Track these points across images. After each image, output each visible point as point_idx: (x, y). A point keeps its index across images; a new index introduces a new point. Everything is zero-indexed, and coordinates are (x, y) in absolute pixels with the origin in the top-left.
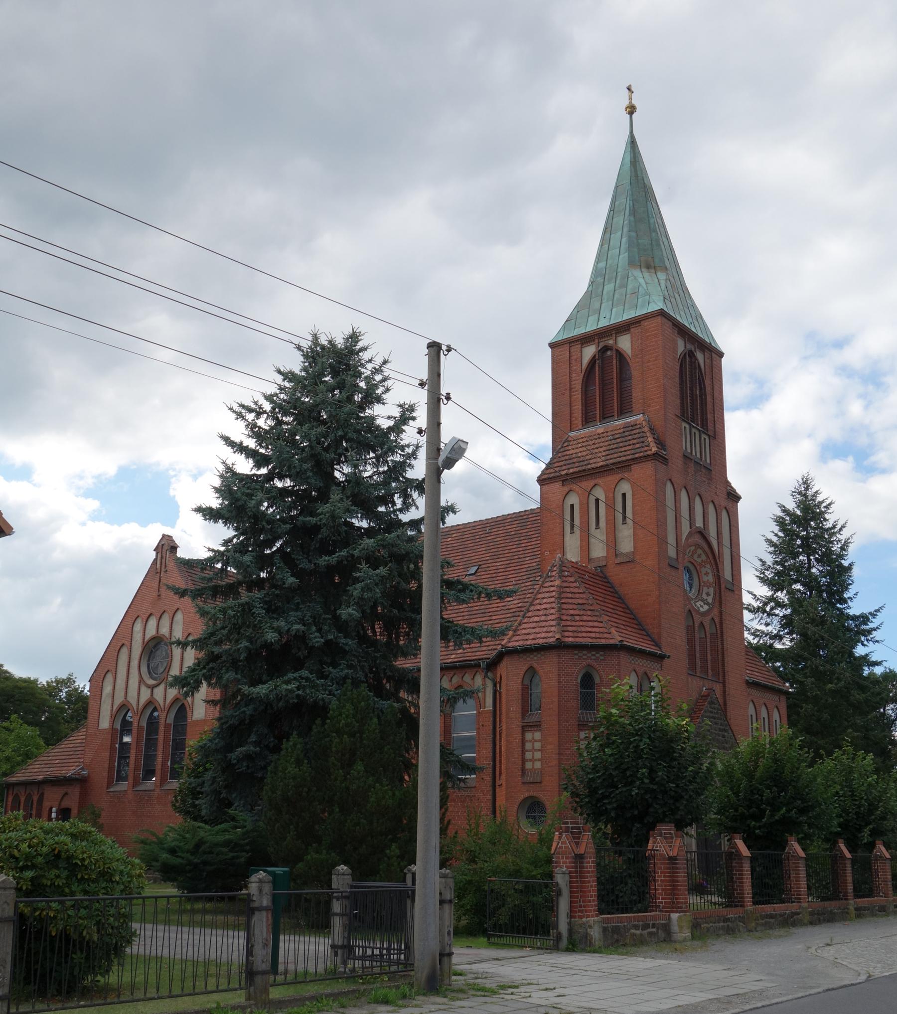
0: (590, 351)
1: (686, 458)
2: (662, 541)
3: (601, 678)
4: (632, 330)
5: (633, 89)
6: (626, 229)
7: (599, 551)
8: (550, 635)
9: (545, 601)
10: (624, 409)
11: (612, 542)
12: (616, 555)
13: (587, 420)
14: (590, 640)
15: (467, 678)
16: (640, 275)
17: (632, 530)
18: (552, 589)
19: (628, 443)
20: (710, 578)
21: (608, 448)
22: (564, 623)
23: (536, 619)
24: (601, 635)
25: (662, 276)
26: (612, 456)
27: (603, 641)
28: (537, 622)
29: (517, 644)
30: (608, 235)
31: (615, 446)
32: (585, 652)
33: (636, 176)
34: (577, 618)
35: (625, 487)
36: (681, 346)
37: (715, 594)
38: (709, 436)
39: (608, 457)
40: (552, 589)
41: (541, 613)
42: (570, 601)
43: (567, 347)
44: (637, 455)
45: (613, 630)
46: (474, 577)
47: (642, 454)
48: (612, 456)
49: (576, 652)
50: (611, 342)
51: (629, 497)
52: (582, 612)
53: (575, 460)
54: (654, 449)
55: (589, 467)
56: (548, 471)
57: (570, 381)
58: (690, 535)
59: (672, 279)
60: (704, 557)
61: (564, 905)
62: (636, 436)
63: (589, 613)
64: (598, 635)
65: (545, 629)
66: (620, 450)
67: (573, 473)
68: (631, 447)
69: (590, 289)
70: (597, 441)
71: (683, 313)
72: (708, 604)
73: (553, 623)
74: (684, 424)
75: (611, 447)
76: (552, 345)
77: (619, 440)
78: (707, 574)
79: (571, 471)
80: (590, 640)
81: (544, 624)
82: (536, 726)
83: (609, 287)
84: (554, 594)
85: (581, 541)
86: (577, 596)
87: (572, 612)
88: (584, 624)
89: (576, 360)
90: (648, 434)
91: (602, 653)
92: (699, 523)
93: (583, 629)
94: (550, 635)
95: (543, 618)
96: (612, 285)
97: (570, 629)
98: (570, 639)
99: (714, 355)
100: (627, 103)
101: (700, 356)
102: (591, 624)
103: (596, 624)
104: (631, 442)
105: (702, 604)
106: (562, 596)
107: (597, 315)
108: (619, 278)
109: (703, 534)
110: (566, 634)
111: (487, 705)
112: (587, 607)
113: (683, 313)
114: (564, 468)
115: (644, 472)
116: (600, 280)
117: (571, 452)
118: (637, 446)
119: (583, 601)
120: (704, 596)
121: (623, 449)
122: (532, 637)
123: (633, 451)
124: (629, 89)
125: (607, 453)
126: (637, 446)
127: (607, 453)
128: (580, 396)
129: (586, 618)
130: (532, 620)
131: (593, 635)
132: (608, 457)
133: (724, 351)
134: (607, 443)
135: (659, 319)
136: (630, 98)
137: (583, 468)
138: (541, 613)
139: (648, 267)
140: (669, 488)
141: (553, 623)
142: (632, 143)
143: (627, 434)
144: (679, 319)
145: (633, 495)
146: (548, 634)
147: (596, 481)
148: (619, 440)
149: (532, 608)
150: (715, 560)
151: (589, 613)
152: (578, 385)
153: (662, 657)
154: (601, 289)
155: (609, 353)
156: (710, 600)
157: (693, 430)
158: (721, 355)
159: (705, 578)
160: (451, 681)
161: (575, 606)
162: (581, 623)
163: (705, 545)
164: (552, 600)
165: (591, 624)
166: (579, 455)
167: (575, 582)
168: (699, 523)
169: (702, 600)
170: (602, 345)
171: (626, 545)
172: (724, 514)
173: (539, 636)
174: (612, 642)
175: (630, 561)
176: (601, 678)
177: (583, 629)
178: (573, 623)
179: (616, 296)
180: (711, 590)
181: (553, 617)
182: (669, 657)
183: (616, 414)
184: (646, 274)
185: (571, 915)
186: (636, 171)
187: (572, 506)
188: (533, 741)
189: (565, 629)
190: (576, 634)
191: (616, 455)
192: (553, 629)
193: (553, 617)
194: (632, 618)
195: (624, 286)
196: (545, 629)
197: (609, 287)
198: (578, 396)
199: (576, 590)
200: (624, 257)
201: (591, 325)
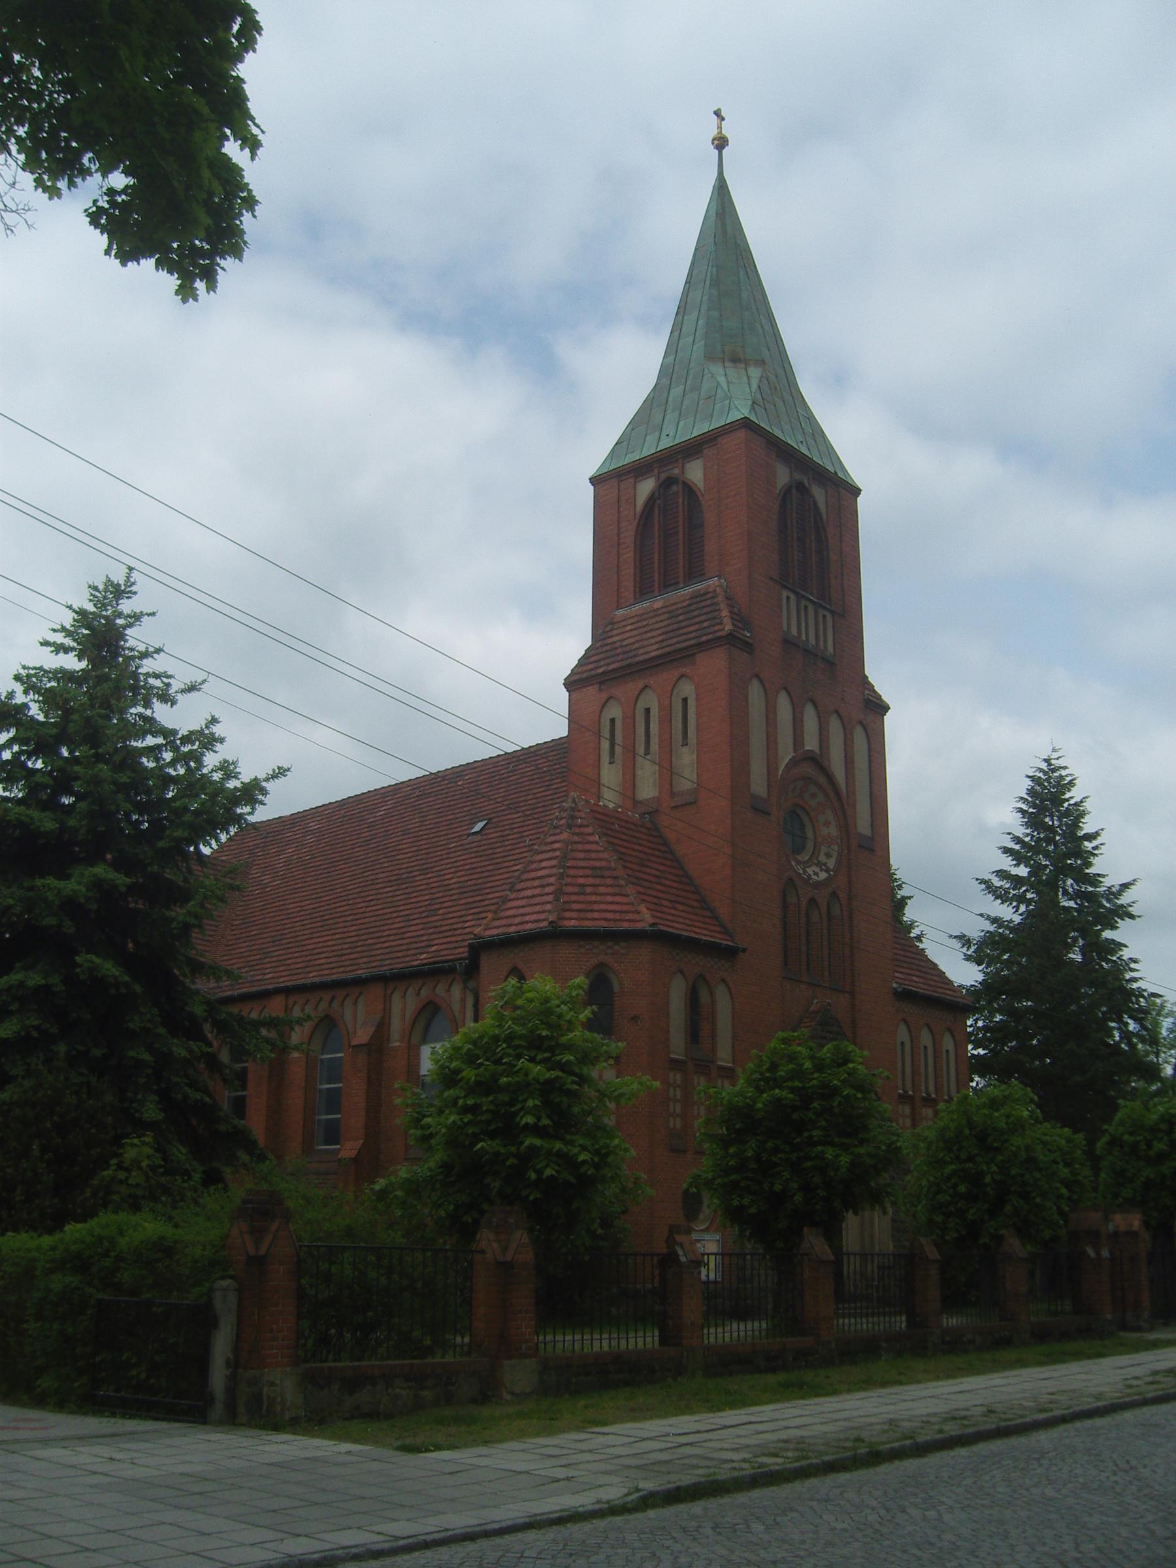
0: (646, 487)
1: (788, 643)
2: (740, 770)
4: (705, 451)
5: (723, 114)
7: (647, 790)
8: (543, 916)
9: (544, 864)
10: (694, 572)
11: (668, 771)
13: (643, 590)
14: (605, 924)
16: (721, 371)
18: (556, 846)
19: (692, 621)
20: (833, 830)
22: (566, 898)
23: (529, 893)
25: (755, 373)
26: (670, 642)
27: (625, 926)
29: (495, 932)
31: (676, 626)
32: (610, 944)
33: (725, 233)
35: (687, 689)
36: (783, 476)
38: (832, 612)
39: (664, 644)
40: (556, 846)
41: (536, 883)
42: (582, 864)
45: (643, 908)
46: (479, 837)
47: (710, 637)
48: (670, 642)
49: (582, 943)
50: (676, 471)
51: (692, 703)
52: (598, 881)
53: (618, 651)
54: (728, 627)
55: (636, 659)
58: (794, 763)
59: (772, 378)
61: (221, 1345)
64: (618, 916)
65: (537, 908)
66: (682, 631)
67: (613, 670)
68: (697, 627)
70: (651, 621)
71: (787, 427)
73: (550, 898)
74: (785, 593)
75: (671, 628)
76: (593, 480)
77: (681, 618)
79: (611, 667)
80: (605, 924)
81: (537, 900)
83: (676, 391)
84: (558, 853)
87: (581, 881)
90: (722, 606)
91: (623, 944)
93: (595, 907)
94: (543, 916)
97: (575, 906)
98: (573, 923)
99: (843, 491)
100: (715, 132)
101: (818, 494)
102: (610, 899)
104: (698, 620)
105: (817, 870)
107: (657, 433)
108: (690, 377)
109: (817, 761)
112: (607, 873)
113: (787, 427)
114: (602, 663)
118: (706, 624)
120: (822, 858)
121: (685, 631)
122: (517, 920)
124: (717, 113)
125: (664, 637)
126: (706, 624)
127: (664, 637)
128: (631, 554)
129: (602, 890)
130: (523, 894)
131: (608, 915)
132: (664, 644)
133: (859, 484)
134: (665, 623)
135: (741, 434)
136: (720, 128)
137: (629, 661)
138: (536, 883)
139: (735, 360)
140: (755, 691)
142: (721, 190)
143: (693, 607)
144: (778, 433)
145: (698, 699)
148: (681, 618)
149: (525, 877)
150: (842, 804)
153: (731, 953)
155: (674, 488)
156: (831, 863)
157: (803, 603)
158: (856, 491)
159: (824, 831)
160: (418, 994)
161: (587, 872)
162: (594, 898)
163: (822, 780)
164: (554, 862)
165: (610, 899)
166: (625, 643)
167: (592, 834)
169: (819, 864)
170: (663, 476)
172: (859, 733)
173: (527, 918)
174: (639, 926)
177: (595, 907)
178: (582, 898)
179: (685, 403)
182: (744, 950)
183: (681, 578)
184: (732, 372)
185: (235, 1364)
186: (724, 225)
187: (613, 721)
190: (582, 915)
191: (674, 640)
192: (548, 907)
195: (696, 388)
196: (537, 908)
197: (676, 391)
198: (629, 555)
200: (700, 346)
201: (648, 450)
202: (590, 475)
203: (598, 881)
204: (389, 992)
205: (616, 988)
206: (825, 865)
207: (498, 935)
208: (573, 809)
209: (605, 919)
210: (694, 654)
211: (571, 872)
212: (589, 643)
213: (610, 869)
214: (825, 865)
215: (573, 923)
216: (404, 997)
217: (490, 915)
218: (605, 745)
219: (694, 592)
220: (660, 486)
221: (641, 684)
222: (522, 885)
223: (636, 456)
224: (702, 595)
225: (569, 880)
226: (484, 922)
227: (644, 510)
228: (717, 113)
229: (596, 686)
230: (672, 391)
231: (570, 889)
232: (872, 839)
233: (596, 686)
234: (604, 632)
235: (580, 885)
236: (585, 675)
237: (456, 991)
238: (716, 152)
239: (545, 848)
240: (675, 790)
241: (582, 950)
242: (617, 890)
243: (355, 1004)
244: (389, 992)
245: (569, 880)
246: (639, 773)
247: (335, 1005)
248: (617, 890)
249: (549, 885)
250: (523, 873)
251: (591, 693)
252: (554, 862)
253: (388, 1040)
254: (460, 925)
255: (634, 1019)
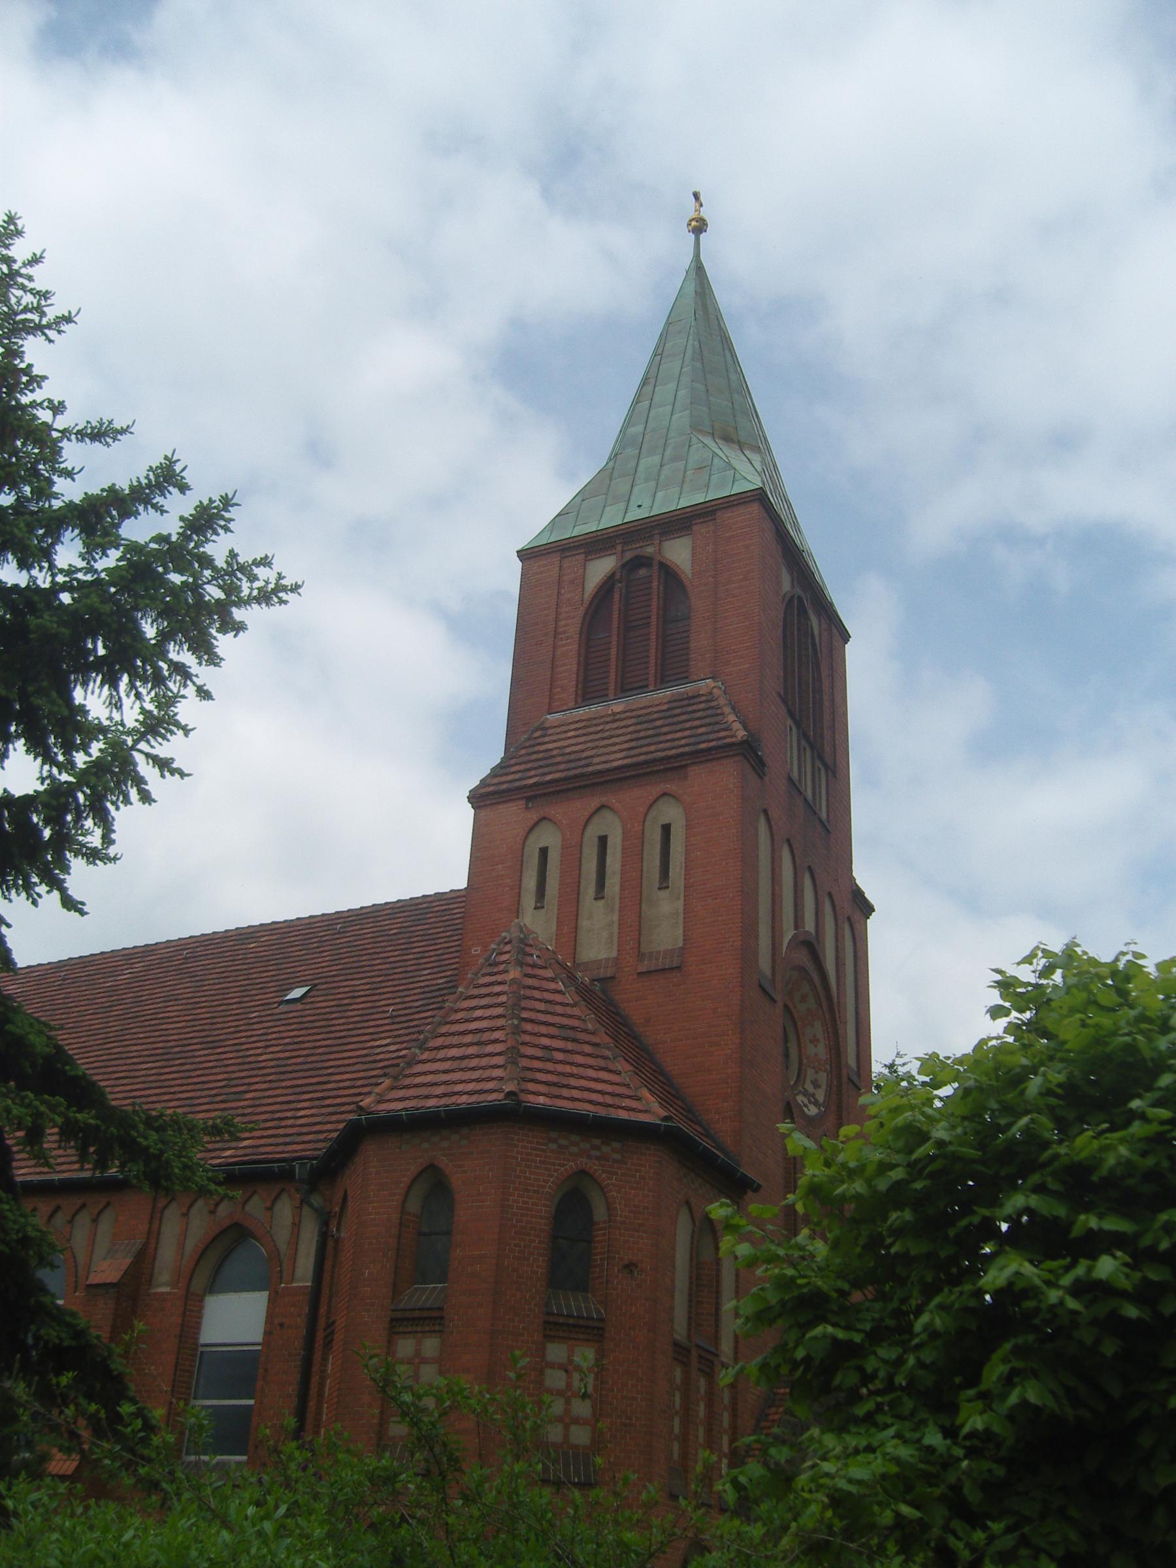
0: (601, 568)
3: (610, 1208)
4: (695, 528)
6: (685, 379)
7: (598, 944)
9: (478, 1013)
10: (673, 667)
12: (641, 956)
13: (588, 692)
15: (256, 1206)
17: (680, 904)
20: (820, 1051)
21: (634, 736)
22: (524, 1062)
24: (617, 1101)
28: (453, 1059)
30: (649, 388)
32: (597, 1142)
34: (559, 1056)
35: (671, 813)
37: (829, 1086)
41: (468, 1039)
43: (555, 559)
44: (703, 746)
46: (299, 1006)
49: (553, 1135)
50: (650, 550)
52: (570, 1046)
55: (590, 769)
56: (496, 780)
57: (557, 620)
60: (812, 1003)
62: (699, 714)
63: (587, 1049)
65: (476, 1075)
67: (549, 782)
69: (611, 464)
70: (607, 727)
72: (816, 1104)
73: (499, 1060)
76: (523, 555)
78: (815, 1041)
81: (474, 1063)
82: (429, 1320)
84: (503, 998)
85: (559, 924)
86: (559, 1009)
87: (546, 1041)
88: (575, 1070)
89: (572, 582)
91: (615, 1145)
92: (809, 926)
93: (573, 1082)
95: (471, 1050)
96: (656, 459)
98: (541, 1099)
102: (591, 1073)
103: (603, 1075)
106: (524, 1004)
110: (531, 1086)
111: (299, 1272)
115: (721, 781)
116: (631, 451)
117: (550, 746)
119: (576, 1023)
120: (809, 1087)
123: (692, 740)
124: (696, 196)
129: (579, 1059)
130: (442, 1054)
138: (468, 1039)
141: (499, 1060)
145: (689, 827)
146: (480, 1082)
147: (604, 800)
151: (587, 1049)
152: (572, 626)
154: (633, 464)
155: (643, 572)
156: (820, 1096)
164: (500, 1011)
165: (591, 1073)
166: (568, 750)
167: (553, 980)
168: (809, 926)
170: (629, 556)
171: (666, 926)
173: (459, 1088)
175: (672, 969)
176: (610, 1208)
177: (573, 1082)
178: (549, 1066)
180: (823, 1077)
181: (499, 1048)
183: (652, 679)
187: (544, 852)
188: (418, 1360)
189: (529, 1075)
190: (555, 1091)
191: (652, 748)
193: (499, 1048)
194: (668, 1090)
197: (650, 462)
198: (570, 648)
199: (558, 998)
200: (682, 419)
201: (612, 518)
202: (519, 548)
203: (570, 1046)
204: (160, 1205)
205: (600, 1213)
206: (813, 1095)
207: (405, 1109)
208: (521, 941)
209: (590, 1102)
210: (685, 766)
211: (528, 1027)
212: (496, 755)
213: (585, 1031)
214: (813, 1095)
215: (541, 1099)
216: (186, 1215)
217: (387, 1082)
218: (530, 882)
219: (672, 695)
220: (623, 566)
221: (594, 803)
222: (439, 1042)
223: (593, 527)
224: (689, 698)
225: (527, 1038)
226: (378, 1090)
227: (595, 596)
228: (696, 196)
229: (523, 802)
230: (642, 461)
231: (530, 1051)
232: (859, 1074)
233: (523, 802)
234: (529, 739)
235: (545, 1048)
236: (504, 787)
237: (285, 1210)
238: (692, 236)
239: (476, 992)
240: (643, 950)
241: (553, 1146)
242: (601, 1063)
243: (95, 1221)
244: (160, 1205)
245: (527, 1038)
246: (584, 923)
247: (60, 1219)
248: (601, 1063)
249: (496, 1041)
250: (440, 1024)
251: (513, 814)
252: (500, 1011)
253: (150, 1282)
254: (289, 1114)
255: (630, 1267)
